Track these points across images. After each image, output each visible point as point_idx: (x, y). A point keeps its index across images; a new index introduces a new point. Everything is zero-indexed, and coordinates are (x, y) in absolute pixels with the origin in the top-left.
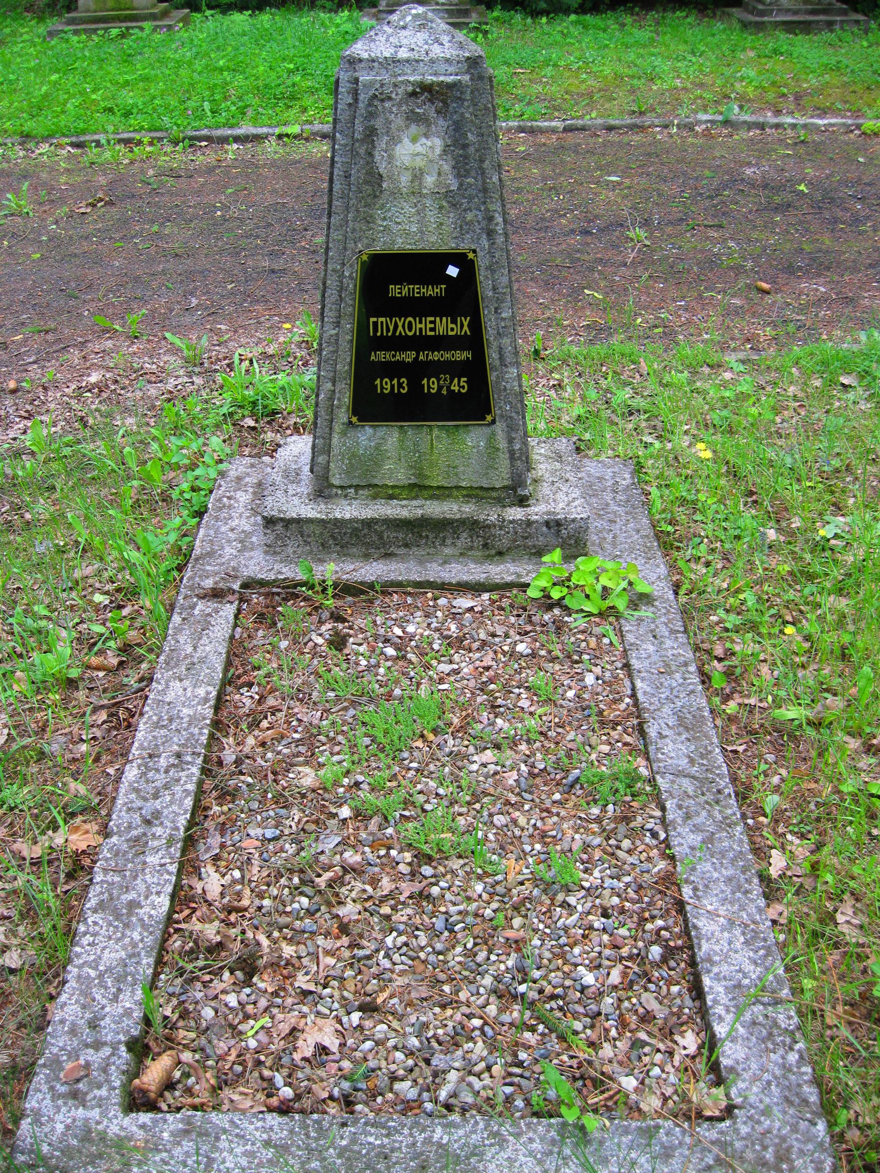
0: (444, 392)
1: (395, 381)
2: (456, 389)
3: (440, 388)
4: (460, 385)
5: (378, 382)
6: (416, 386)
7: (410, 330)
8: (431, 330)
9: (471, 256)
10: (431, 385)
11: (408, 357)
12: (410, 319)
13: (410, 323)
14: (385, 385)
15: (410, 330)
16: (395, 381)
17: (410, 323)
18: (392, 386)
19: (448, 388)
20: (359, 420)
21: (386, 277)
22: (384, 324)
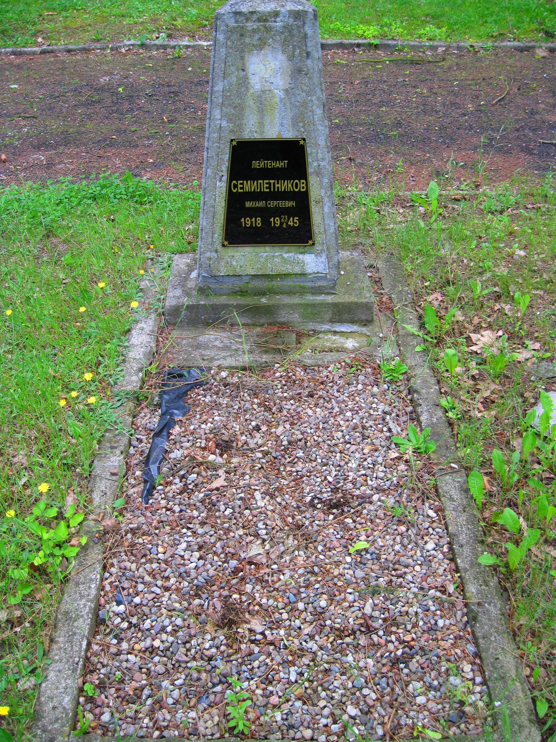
0: (284, 226)
1: (253, 220)
2: (292, 224)
3: (282, 224)
4: (294, 222)
5: (272, 219)
6: (266, 222)
7: (297, 187)
8: (241, 188)
9: (234, 143)
10: (276, 222)
11: (261, 204)
12: (297, 181)
13: (297, 184)
14: (247, 222)
15: (297, 187)
16: (253, 220)
17: (297, 184)
18: (252, 223)
19: (287, 223)
20: (229, 243)
21: (246, 156)
22: (249, 186)
